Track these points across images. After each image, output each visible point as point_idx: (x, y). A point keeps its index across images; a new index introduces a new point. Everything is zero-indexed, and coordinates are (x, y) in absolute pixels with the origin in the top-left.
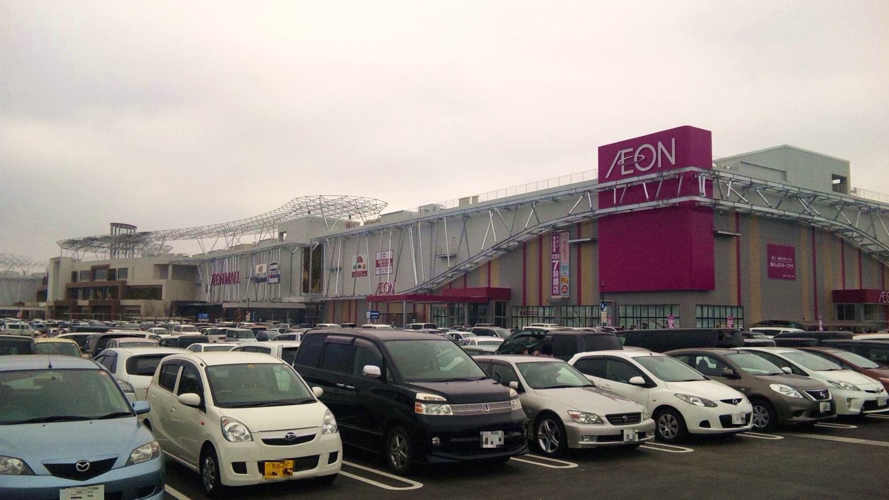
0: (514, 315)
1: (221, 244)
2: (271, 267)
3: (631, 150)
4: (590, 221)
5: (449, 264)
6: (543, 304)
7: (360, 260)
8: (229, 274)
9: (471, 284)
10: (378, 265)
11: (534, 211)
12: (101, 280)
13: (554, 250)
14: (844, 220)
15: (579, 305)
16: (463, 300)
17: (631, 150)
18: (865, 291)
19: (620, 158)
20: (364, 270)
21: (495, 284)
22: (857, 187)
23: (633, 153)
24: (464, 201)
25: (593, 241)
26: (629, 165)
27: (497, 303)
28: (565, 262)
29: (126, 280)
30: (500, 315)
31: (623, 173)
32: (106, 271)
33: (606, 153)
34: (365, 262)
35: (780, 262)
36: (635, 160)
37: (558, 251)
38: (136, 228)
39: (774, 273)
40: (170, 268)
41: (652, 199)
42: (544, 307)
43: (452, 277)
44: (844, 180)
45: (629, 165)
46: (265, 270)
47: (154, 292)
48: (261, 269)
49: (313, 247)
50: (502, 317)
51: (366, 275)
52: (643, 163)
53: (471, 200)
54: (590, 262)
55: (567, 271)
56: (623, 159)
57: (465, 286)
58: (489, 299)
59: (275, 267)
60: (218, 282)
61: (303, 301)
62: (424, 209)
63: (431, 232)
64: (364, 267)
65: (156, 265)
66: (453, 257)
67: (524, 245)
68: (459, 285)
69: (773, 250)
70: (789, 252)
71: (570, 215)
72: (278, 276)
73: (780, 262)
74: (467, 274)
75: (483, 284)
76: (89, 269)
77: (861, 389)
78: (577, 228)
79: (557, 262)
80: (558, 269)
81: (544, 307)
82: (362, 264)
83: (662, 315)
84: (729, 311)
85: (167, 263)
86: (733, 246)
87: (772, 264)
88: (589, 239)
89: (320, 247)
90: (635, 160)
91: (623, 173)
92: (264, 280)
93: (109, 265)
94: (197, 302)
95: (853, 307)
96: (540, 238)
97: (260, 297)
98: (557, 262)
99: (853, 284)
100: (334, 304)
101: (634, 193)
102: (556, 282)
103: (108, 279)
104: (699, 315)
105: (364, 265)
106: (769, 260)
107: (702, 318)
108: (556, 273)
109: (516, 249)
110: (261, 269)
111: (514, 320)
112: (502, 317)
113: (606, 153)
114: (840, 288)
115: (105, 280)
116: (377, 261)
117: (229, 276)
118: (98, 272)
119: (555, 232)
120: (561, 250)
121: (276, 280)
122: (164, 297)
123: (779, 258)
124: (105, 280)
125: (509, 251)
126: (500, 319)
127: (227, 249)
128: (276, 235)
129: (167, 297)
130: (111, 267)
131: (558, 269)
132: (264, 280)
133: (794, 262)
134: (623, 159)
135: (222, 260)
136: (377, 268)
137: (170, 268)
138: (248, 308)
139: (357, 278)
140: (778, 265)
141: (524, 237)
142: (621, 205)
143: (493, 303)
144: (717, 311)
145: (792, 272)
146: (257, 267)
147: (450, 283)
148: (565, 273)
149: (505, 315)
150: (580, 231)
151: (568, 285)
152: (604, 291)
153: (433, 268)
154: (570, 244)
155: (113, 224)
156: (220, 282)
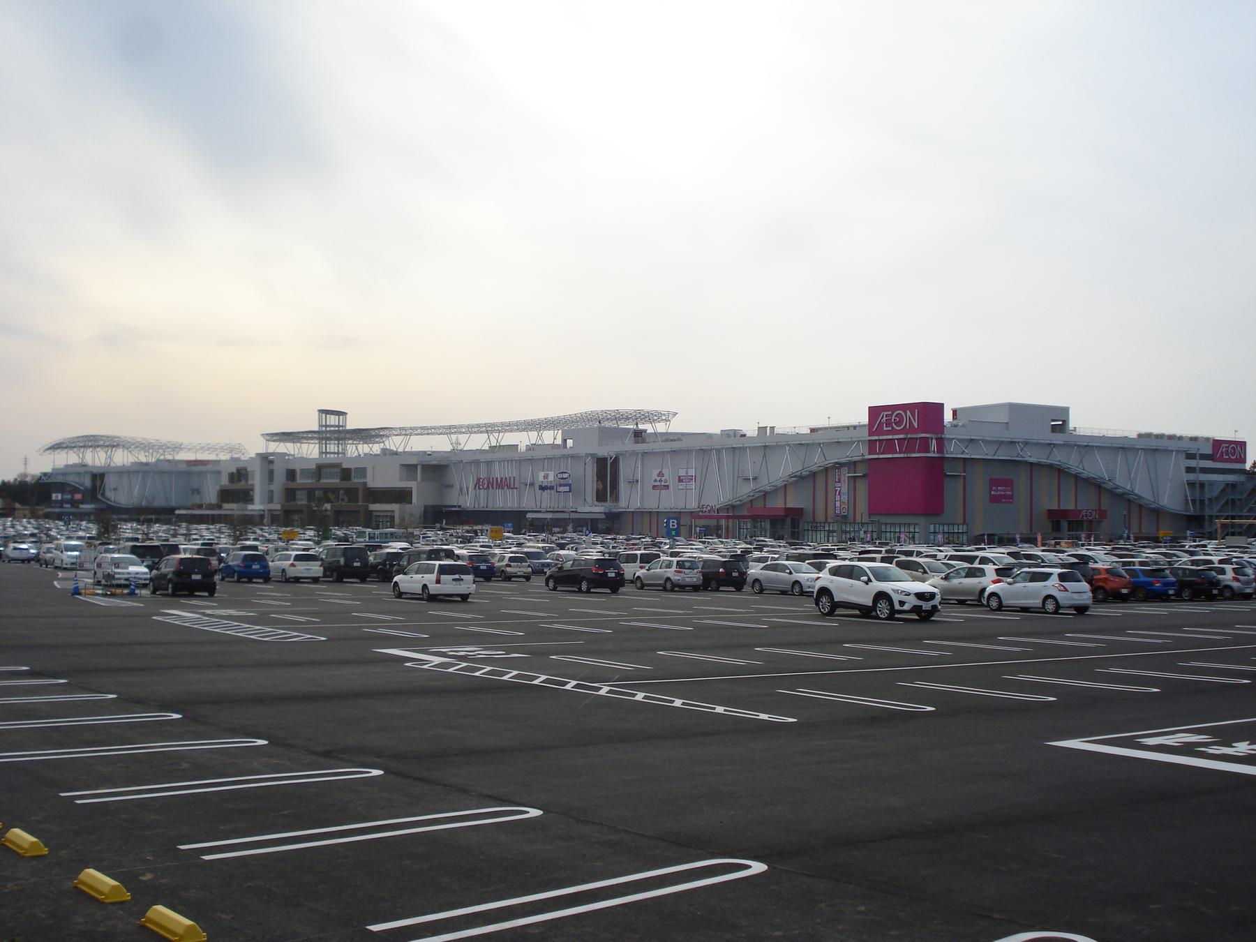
0: (806, 528)
1: (477, 442)
2: (560, 476)
3: (890, 413)
4: (863, 461)
5: (752, 486)
6: (829, 521)
7: (661, 474)
8: (502, 478)
9: (770, 505)
10: (680, 480)
11: (822, 450)
12: (333, 481)
13: (837, 480)
14: (1057, 458)
15: (854, 523)
16: (763, 517)
17: (890, 413)
18: (1080, 511)
19: (882, 418)
20: (666, 484)
21: (790, 505)
22: (1077, 426)
23: (891, 415)
24: (762, 430)
25: (864, 476)
26: (889, 424)
27: (792, 519)
28: (845, 490)
29: (365, 481)
30: (794, 528)
31: (885, 429)
32: (339, 470)
33: (874, 412)
34: (666, 477)
35: (1000, 491)
36: (893, 420)
37: (839, 482)
38: (346, 414)
39: (994, 499)
40: (419, 468)
41: (900, 453)
42: (829, 523)
43: (753, 496)
44: (1065, 422)
45: (889, 424)
46: (551, 478)
47: (402, 496)
48: (546, 477)
49: (611, 458)
50: (796, 530)
51: (668, 489)
52: (898, 424)
53: (768, 428)
54: (863, 489)
55: (846, 497)
56: (885, 418)
57: (765, 505)
58: (786, 516)
59: (565, 476)
60: (485, 486)
61: (603, 511)
62: (727, 434)
63: (734, 456)
64: (666, 481)
65: (402, 465)
66: (755, 479)
67: (813, 475)
68: (759, 504)
69: (994, 483)
70: (1008, 483)
71: (847, 457)
72: (570, 485)
73: (1000, 491)
74: (765, 495)
75: (780, 505)
76: (314, 467)
77: (1068, 589)
78: (853, 465)
79: (839, 489)
80: (839, 494)
81: (829, 523)
82: (663, 479)
83: (898, 531)
84: (956, 527)
85: (416, 463)
86: (961, 481)
87: (993, 493)
88: (861, 475)
89: (616, 461)
90: (893, 420)
91: (885, 429)
92: (551, 488)
93: (341, 464)
94: (455, 506)
95: (1060, 521)
96: (827, 469)
97: (544, 505)
98: (839, 489)
99: (1069, 505)
100: (633, 514)
101: (889, 447)
102: (838, 504)
103: (341, 480)
104: (932, 530)
105: (666, 480)
106: (991, 489)
107: (935, 533)
108: (838, 498)
109: (808, 476)
110: (546, 477)
111: (806, 532)
112: (796, 530)
113: (874, 412)
114: (1055, 507)
115: (338, 481)
116: (679, 477)
117: (501, 481)
118: (324, 470)
119: (839, 466)
120: (842, 479)
121: (567, 489)
122: (414, 500)
123: (999, 488)
124: (338, 481)
125: (801, 478)
126: (795, 532)
127: (486, 447)
128: (559, 441)
129: (418, 502)
130: (344, 466)
131: (839, 494)
132: (551, 488)
133: (1012, 490)
134: (885, 418)
135: (489, 463)
136: (680, 483)
137: (419, 468)
138: (569, 519)
139: (661, 491)
140: (999, 493)
141: (814, 469)
142: (881, 454)
143: (789, 520)
144: (946, 527)
145: (1011, 497)
146: (541, 474)
147: (751, 500)
148: (845, 498)
149: (798, 528)
150: (855, 467)
151: (847, 507)
152: (872, 512)
153: (736, 486)
154: (848, 477)
155: (321, 411)
156: (488, 487)
